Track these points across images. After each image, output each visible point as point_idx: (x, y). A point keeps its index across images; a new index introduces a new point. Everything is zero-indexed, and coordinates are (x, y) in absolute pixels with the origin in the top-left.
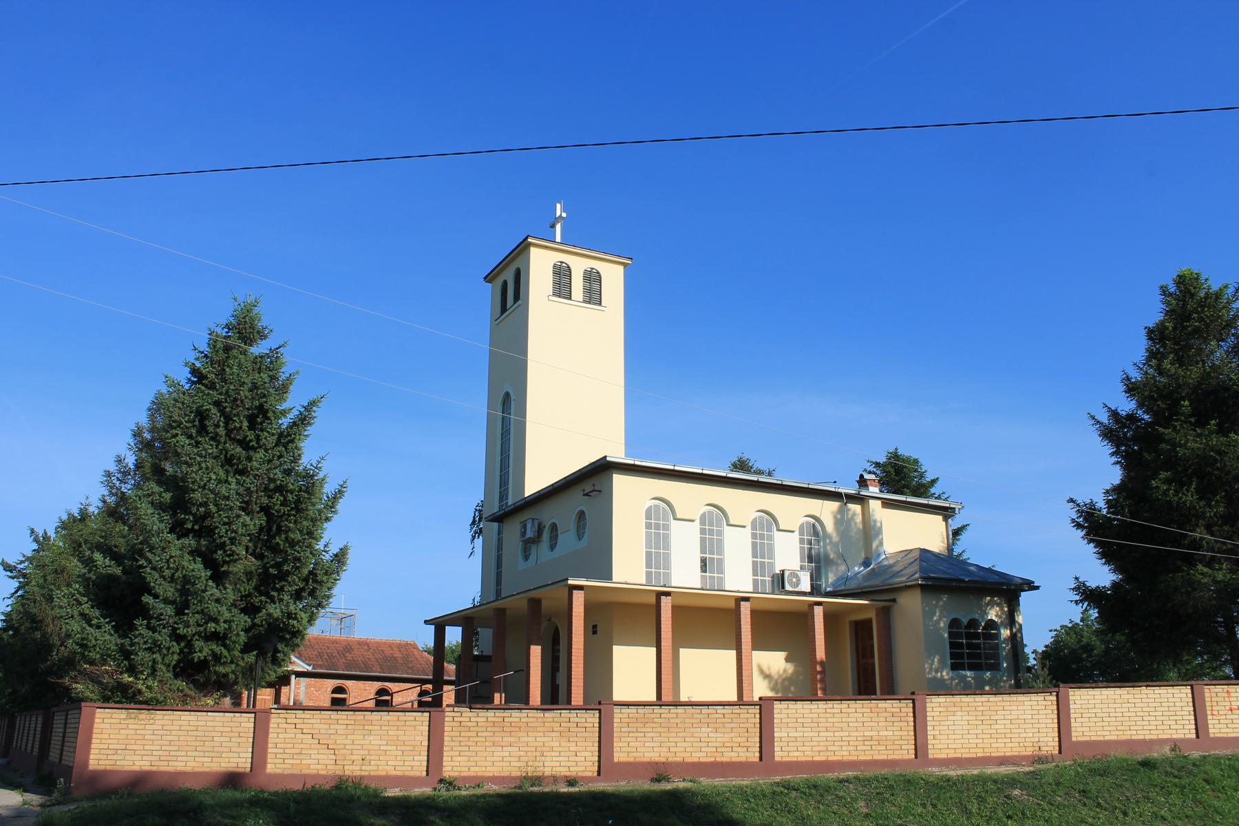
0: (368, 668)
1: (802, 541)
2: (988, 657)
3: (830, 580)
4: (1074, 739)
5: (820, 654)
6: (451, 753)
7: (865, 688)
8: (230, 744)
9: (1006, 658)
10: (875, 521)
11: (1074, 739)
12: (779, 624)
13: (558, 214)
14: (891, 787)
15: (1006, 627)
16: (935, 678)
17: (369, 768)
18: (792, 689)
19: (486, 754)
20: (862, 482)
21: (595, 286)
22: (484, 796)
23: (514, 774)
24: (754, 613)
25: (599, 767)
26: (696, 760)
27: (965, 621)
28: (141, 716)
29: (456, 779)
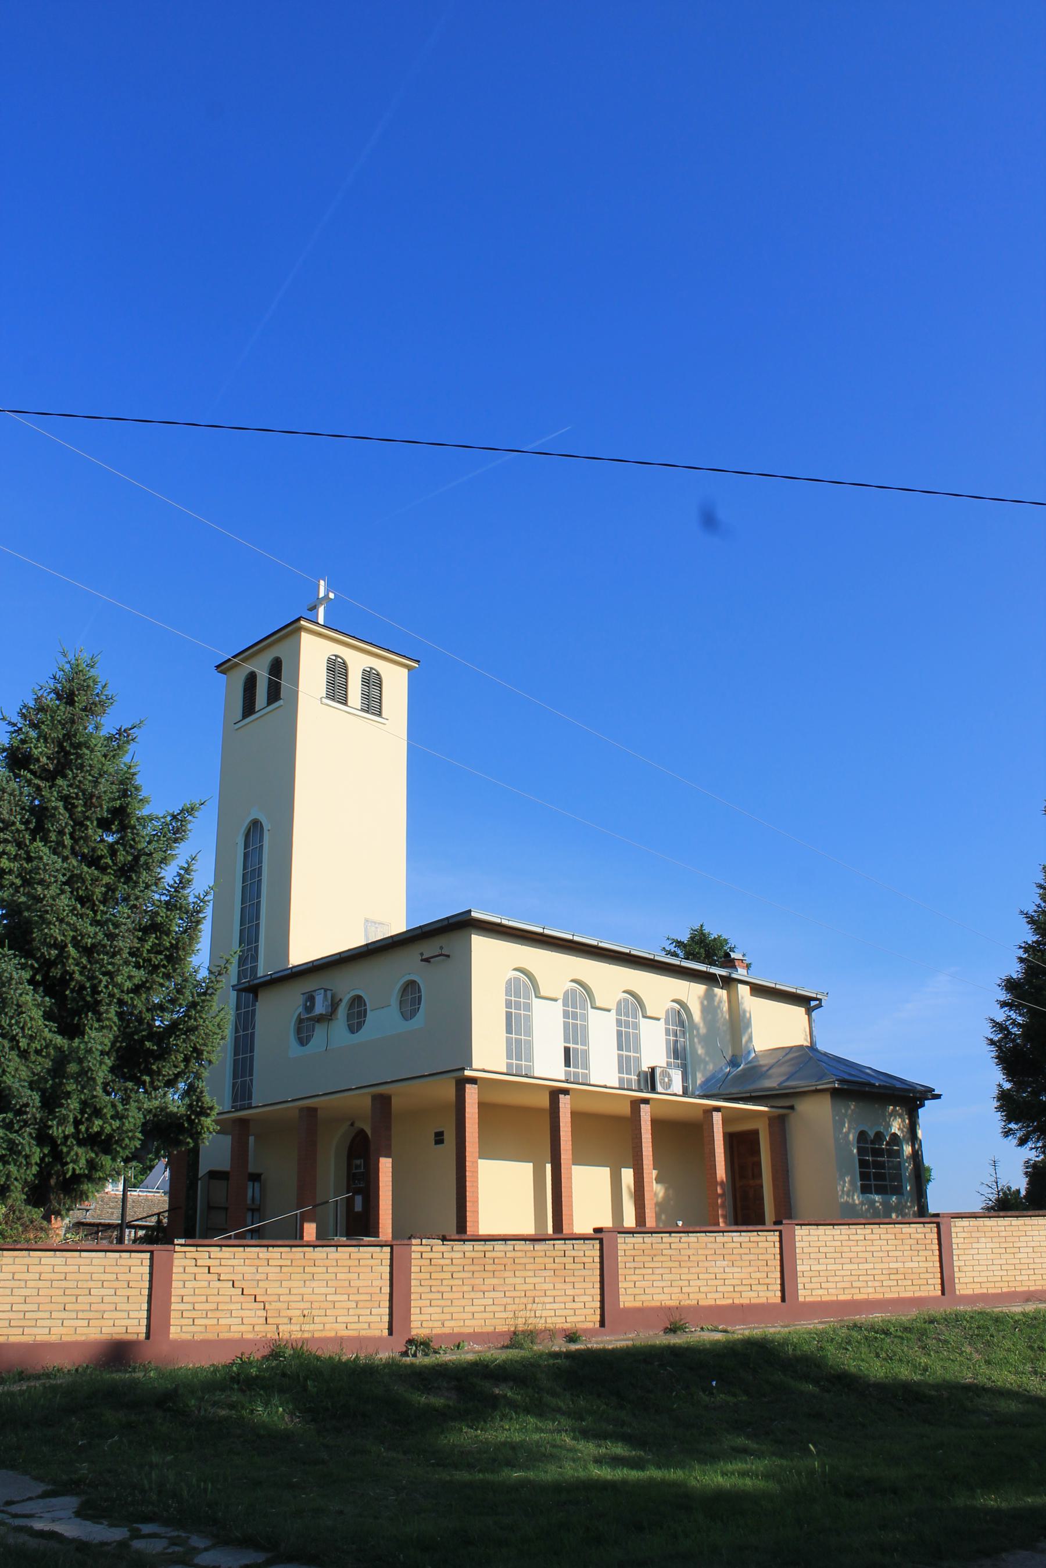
3: (699, 1082)
6: (420, 1303)
7: (746, 1212)
8: (115, 1299)
10: (744, 1011)
13: (322, 594)
16: (847, 1202)
17: (312, 1327)
19: (463, 1302)
21: (375, 692)
23: (499, 1329)
24: (655, 1122)
25: (602, 1315)
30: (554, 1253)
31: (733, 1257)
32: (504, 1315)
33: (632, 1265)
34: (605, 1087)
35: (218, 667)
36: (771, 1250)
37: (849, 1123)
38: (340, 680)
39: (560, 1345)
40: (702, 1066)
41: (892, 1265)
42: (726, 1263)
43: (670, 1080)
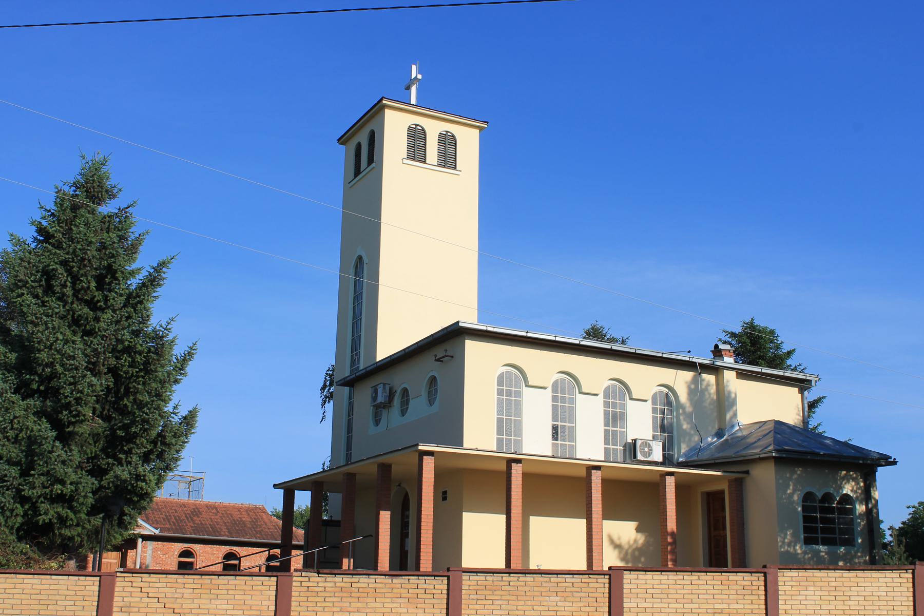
0: (215, 531)
1: (654, 411)
3: (683, 451)
5: (672, 524)
10: (729, 392)
12: (630, 494)
15: (861, 503)
16: (787, 552)
18: (643, 559)
21: (450, 150)
24: (605, 482)
27: (819, 495)
31: (565, 594)
33: (475, 597)
35: (339, 140)
36: (602, 590)
37: (794, 485)
40: (687, 438)
41: (716, 606)
43: (651, 450)
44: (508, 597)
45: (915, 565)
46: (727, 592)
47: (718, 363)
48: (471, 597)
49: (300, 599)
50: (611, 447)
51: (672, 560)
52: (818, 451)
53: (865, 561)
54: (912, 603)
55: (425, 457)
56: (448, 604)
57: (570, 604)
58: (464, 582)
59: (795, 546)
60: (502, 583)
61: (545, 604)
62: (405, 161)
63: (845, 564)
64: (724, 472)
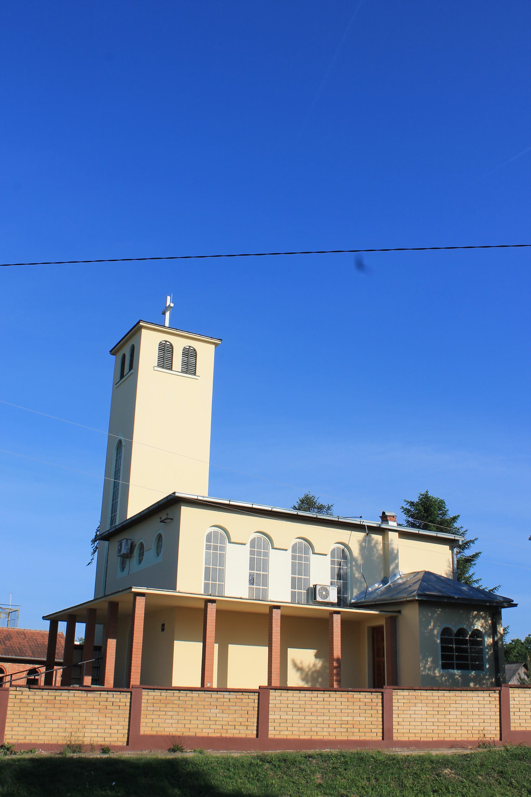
0: (22, 653)
1: (333, 563)
2: (474, 659)
3: (355, 594)
4: (512, 729)
5: (337, 652)
9: (489, 661)
10: (393, 549)
11: (512, 729)
12: (305, 627)
14: (346, 763)
15: (489, 636)
18: (320, 680)
20: (384, 518)
21: (192, 360)
22: (19, 760)
23: (60, 742)
24: (284, 618)
25: (128, 738)
26: (205, 735)
27: (455, 630)
28: (527, 692)
29: (13, 745)
30: (100, 699)
31: (223, 707)
32: (64, 734)
33: (152, 709)
34: (241, 598)
35: (111, 351)
36: (253, 705)
37: (434, 622)
38: (168, 355)
39: (98, 755)
40: (358, 585)
41: (343, 718)
42: (218, 710)
44: (178, 709)
45: (501, 687)
46: (352, 707)
47: (384, 526)
48: (149, 709)
49: (15, 708)
50: (297, 590)
51: (337, 681)
52: (453, 595)
53: (492, 683)
54: (498, 717)
55: (138, 597)
56: (130, 714)
57: (227, 716)
58: (143, 697)
59: (434, 670)
60: (173, 698)
61: (207, 715)
62: (156, 368)
63: (475, 685)
64: (380, 611)
